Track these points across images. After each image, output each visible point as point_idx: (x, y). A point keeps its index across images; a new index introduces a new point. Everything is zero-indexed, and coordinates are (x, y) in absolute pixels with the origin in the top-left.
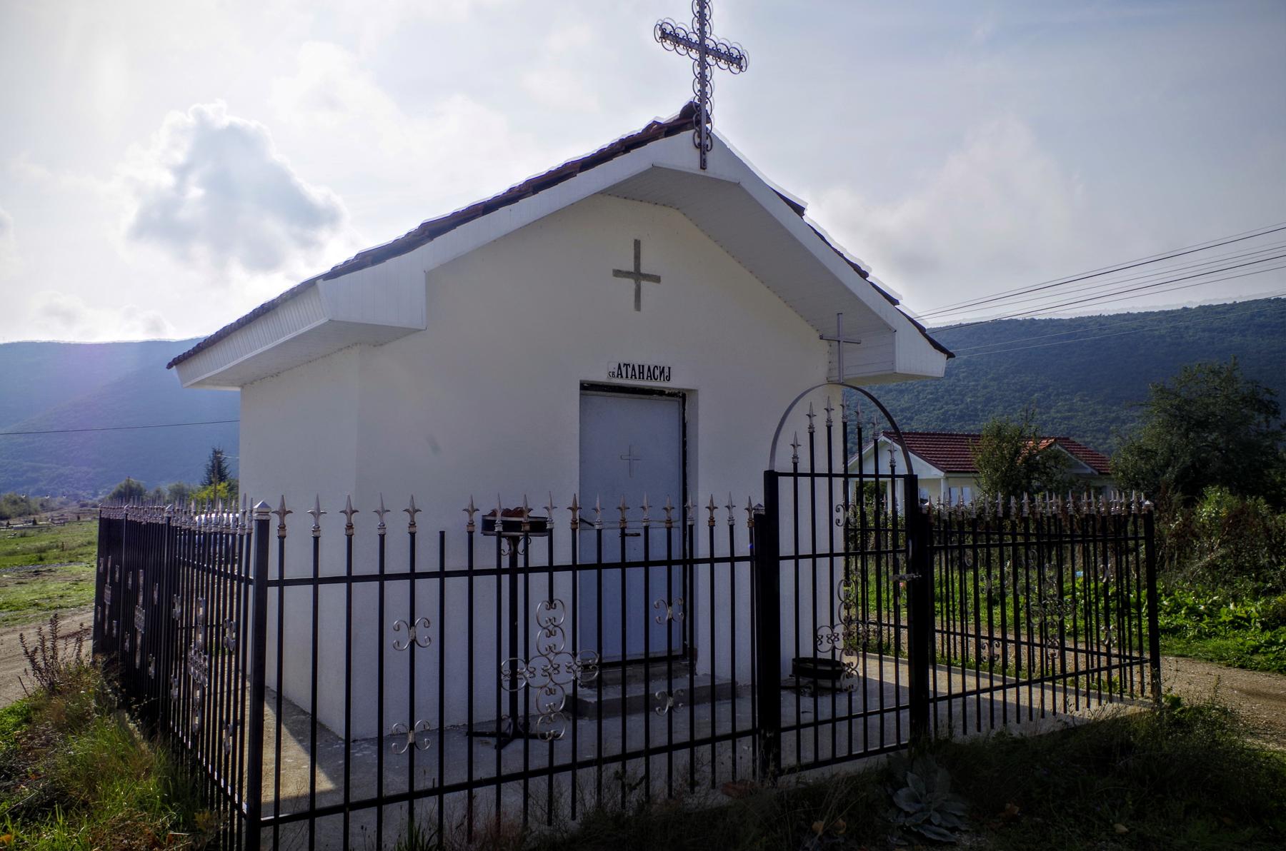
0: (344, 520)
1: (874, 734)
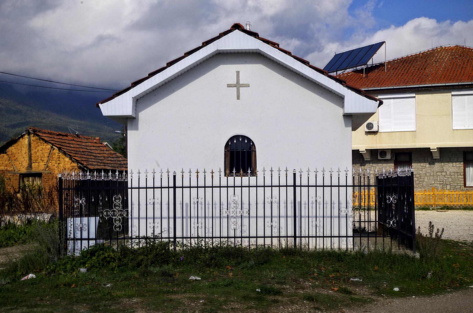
0: (315, 173)
1: (246, 228)
